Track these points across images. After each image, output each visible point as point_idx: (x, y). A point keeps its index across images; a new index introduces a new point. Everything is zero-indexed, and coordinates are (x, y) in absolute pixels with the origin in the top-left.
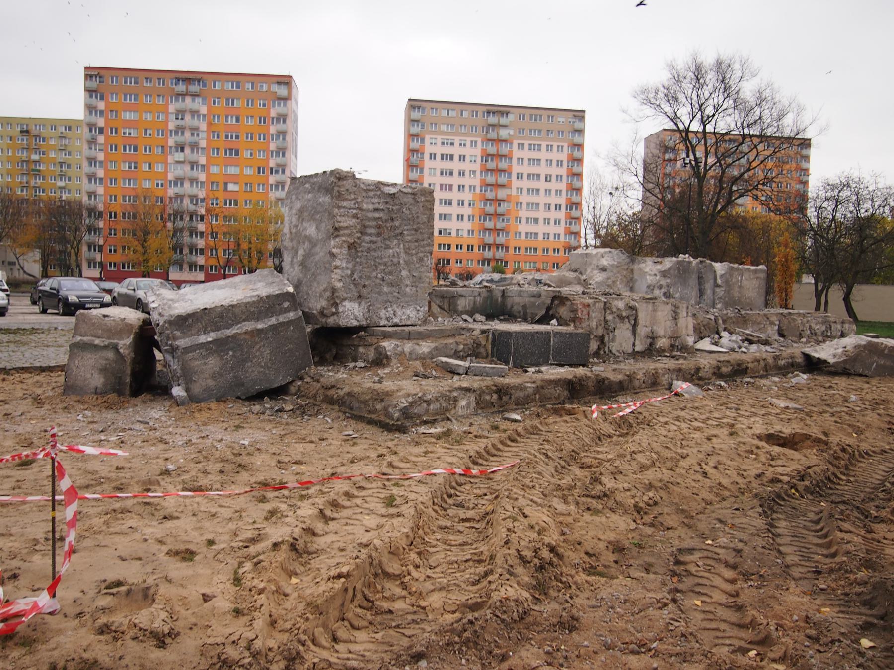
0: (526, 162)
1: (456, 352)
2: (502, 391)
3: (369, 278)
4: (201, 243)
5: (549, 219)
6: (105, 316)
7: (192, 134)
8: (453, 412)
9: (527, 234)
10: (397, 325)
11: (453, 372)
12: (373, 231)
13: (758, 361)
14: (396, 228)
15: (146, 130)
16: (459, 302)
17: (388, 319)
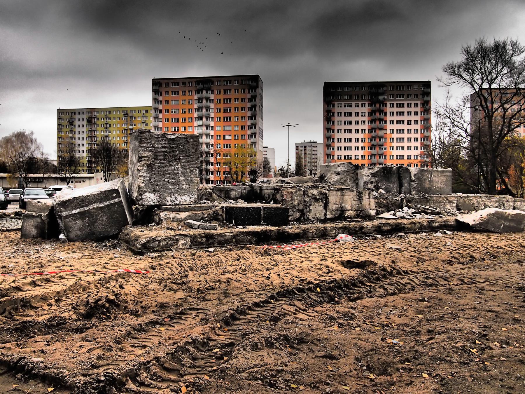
0: (395, 114)
1: (202, 218)
2: (208, 237)
3: (160, 181)
4: (212, 169)
5: (410, 147)
6: (39, 202)
7: (207, 110)
8: (175, 247)
9: (397, 156)
10: (178, 205)
11: (191, 227)
12: (161, 158)
13: (415, 224)
14: (175, 156)
15: (183, 110)
16: (231, 193)
17: (172, 201)
